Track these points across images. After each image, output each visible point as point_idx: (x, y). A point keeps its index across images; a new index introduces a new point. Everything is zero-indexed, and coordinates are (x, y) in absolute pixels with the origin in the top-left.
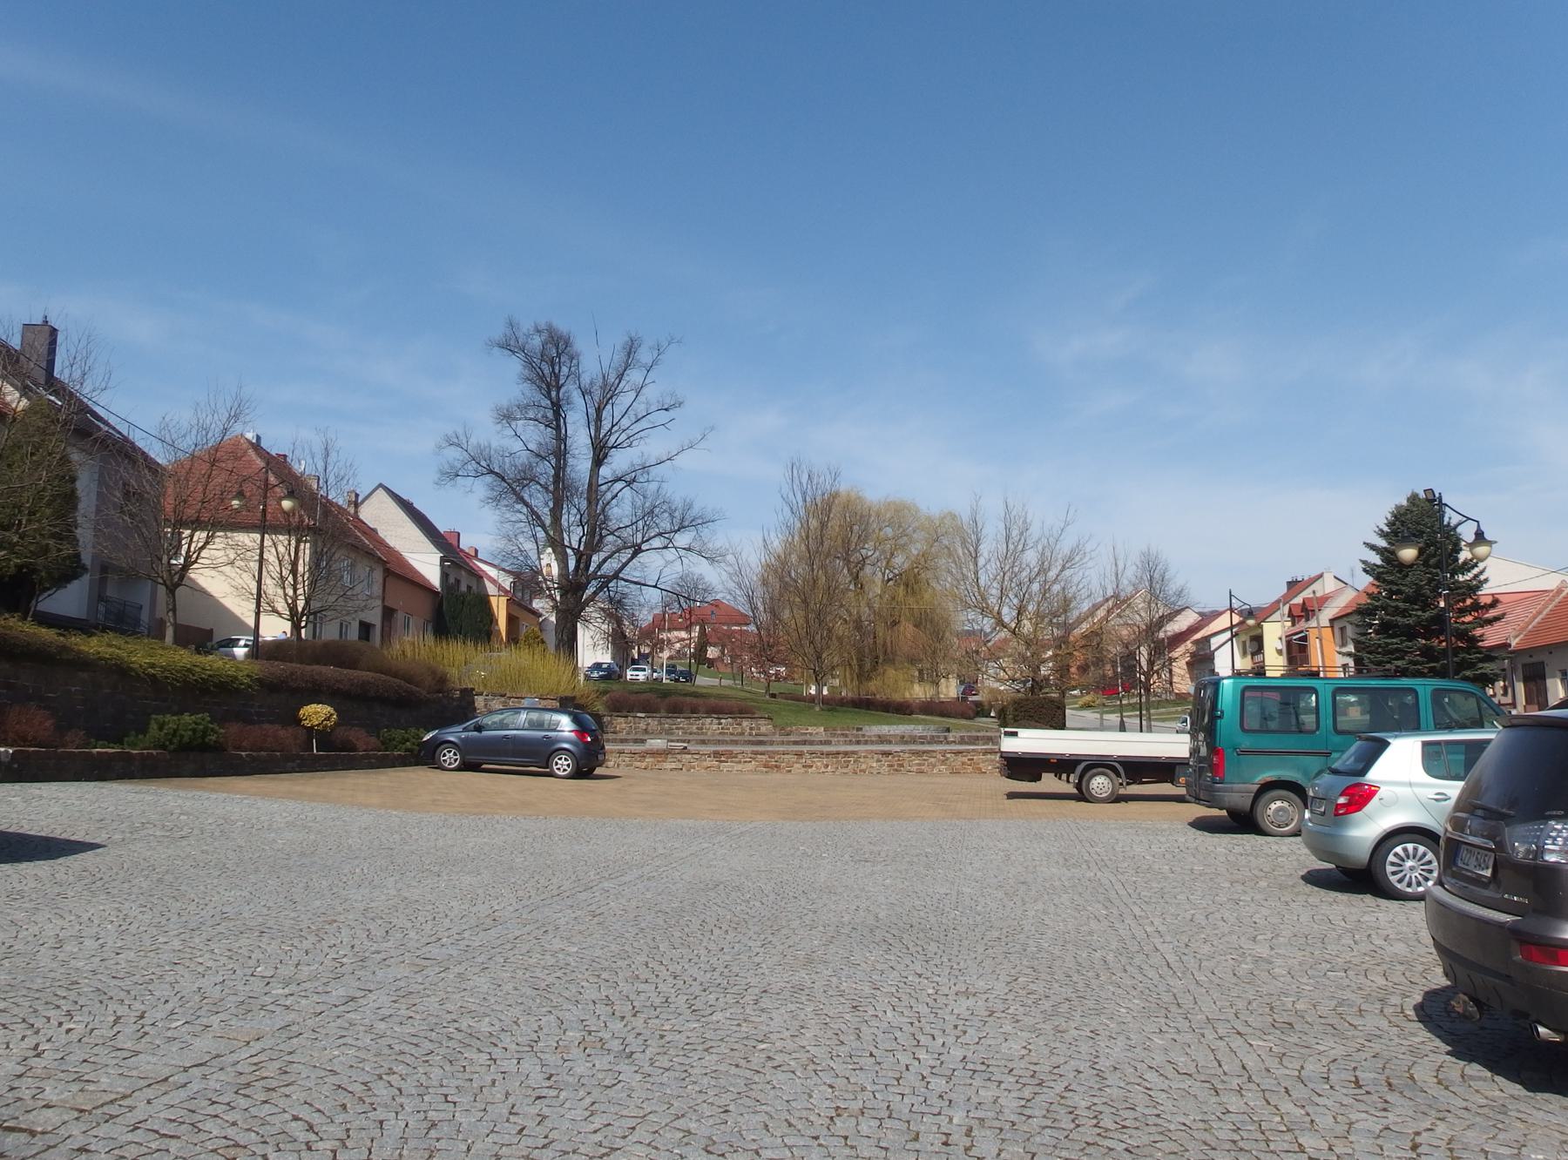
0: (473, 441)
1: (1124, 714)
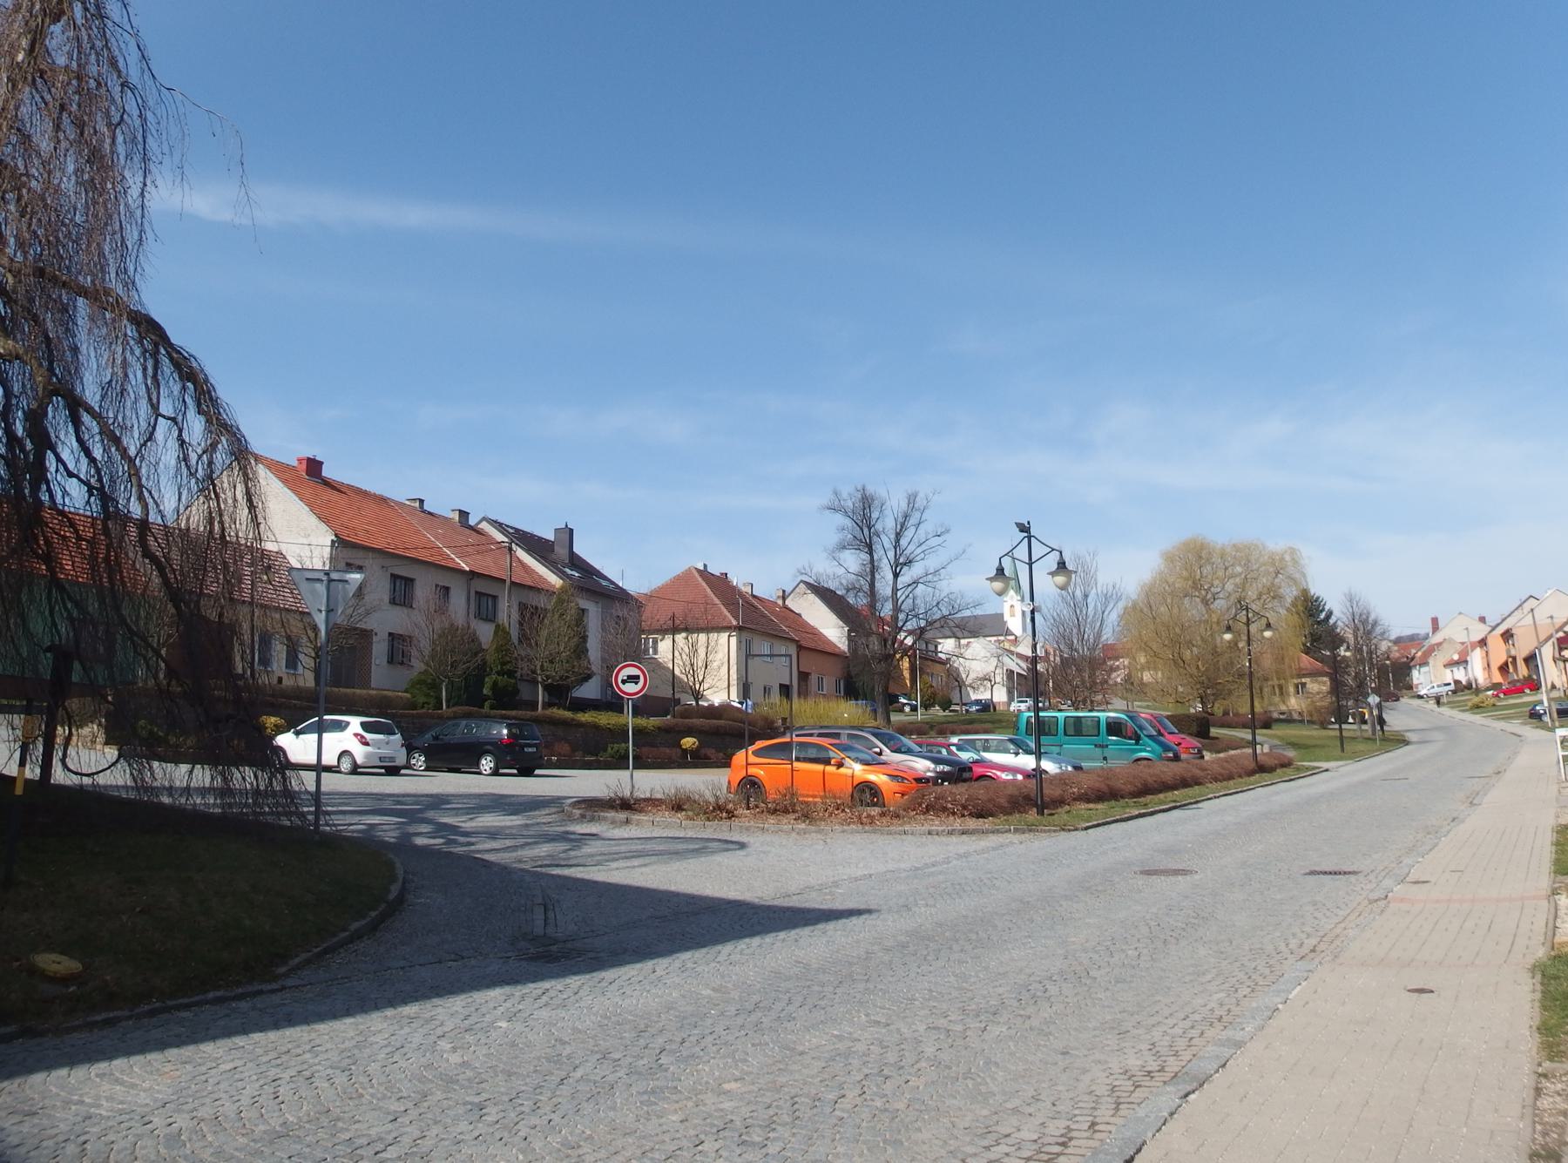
0: (814, 571)
1: (1257, 731)
